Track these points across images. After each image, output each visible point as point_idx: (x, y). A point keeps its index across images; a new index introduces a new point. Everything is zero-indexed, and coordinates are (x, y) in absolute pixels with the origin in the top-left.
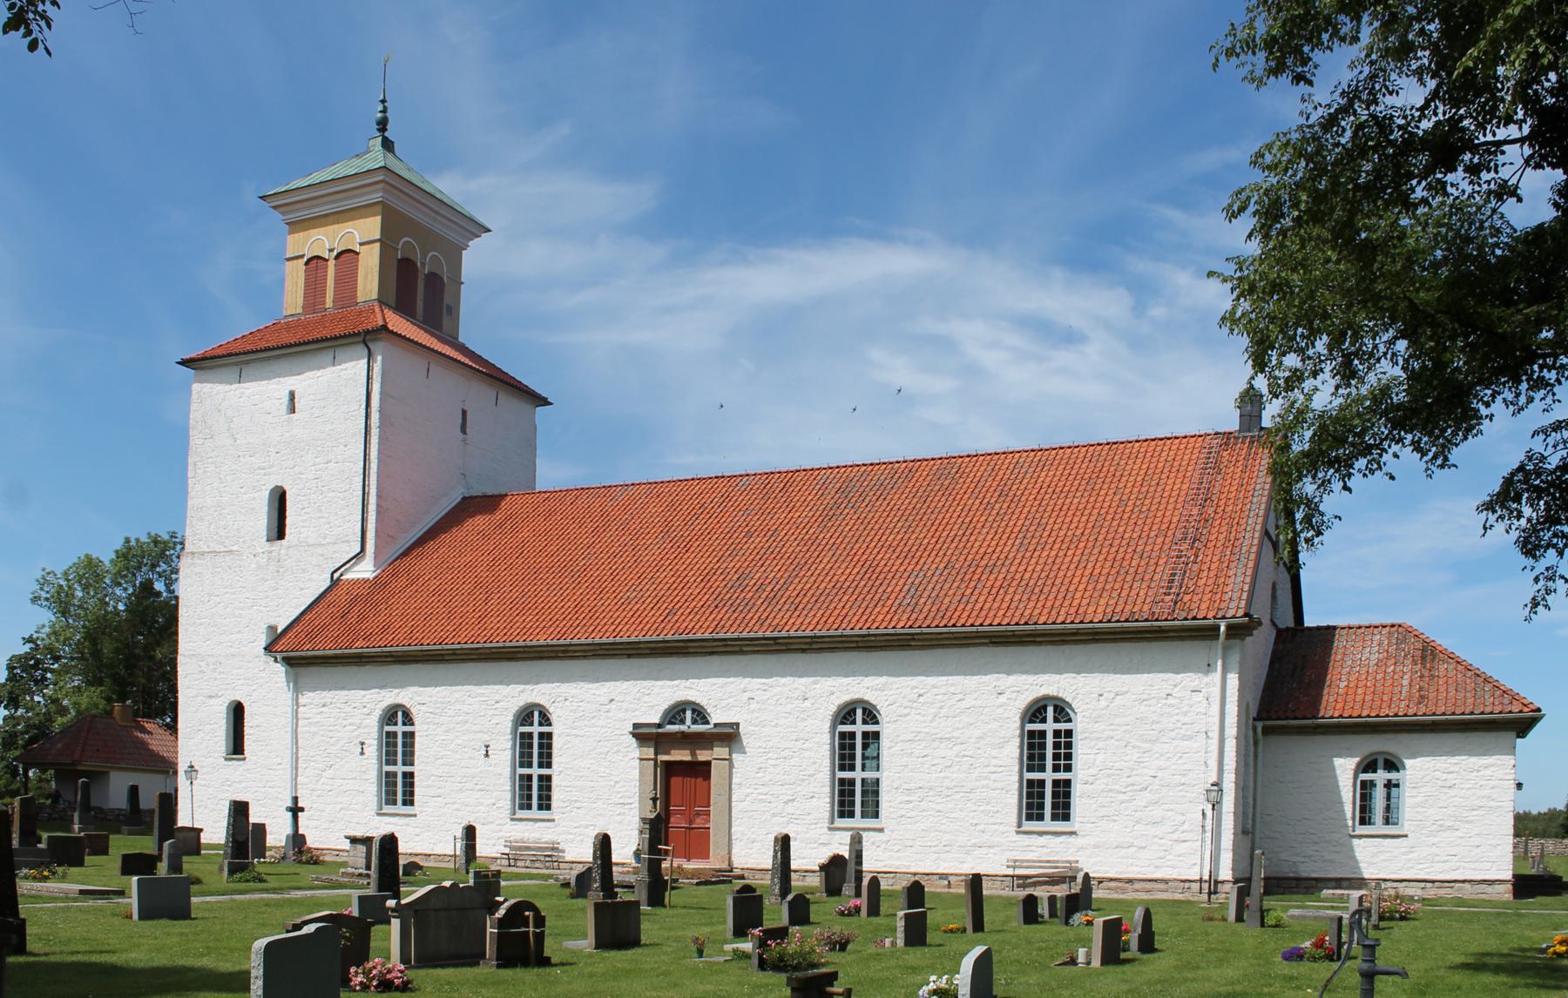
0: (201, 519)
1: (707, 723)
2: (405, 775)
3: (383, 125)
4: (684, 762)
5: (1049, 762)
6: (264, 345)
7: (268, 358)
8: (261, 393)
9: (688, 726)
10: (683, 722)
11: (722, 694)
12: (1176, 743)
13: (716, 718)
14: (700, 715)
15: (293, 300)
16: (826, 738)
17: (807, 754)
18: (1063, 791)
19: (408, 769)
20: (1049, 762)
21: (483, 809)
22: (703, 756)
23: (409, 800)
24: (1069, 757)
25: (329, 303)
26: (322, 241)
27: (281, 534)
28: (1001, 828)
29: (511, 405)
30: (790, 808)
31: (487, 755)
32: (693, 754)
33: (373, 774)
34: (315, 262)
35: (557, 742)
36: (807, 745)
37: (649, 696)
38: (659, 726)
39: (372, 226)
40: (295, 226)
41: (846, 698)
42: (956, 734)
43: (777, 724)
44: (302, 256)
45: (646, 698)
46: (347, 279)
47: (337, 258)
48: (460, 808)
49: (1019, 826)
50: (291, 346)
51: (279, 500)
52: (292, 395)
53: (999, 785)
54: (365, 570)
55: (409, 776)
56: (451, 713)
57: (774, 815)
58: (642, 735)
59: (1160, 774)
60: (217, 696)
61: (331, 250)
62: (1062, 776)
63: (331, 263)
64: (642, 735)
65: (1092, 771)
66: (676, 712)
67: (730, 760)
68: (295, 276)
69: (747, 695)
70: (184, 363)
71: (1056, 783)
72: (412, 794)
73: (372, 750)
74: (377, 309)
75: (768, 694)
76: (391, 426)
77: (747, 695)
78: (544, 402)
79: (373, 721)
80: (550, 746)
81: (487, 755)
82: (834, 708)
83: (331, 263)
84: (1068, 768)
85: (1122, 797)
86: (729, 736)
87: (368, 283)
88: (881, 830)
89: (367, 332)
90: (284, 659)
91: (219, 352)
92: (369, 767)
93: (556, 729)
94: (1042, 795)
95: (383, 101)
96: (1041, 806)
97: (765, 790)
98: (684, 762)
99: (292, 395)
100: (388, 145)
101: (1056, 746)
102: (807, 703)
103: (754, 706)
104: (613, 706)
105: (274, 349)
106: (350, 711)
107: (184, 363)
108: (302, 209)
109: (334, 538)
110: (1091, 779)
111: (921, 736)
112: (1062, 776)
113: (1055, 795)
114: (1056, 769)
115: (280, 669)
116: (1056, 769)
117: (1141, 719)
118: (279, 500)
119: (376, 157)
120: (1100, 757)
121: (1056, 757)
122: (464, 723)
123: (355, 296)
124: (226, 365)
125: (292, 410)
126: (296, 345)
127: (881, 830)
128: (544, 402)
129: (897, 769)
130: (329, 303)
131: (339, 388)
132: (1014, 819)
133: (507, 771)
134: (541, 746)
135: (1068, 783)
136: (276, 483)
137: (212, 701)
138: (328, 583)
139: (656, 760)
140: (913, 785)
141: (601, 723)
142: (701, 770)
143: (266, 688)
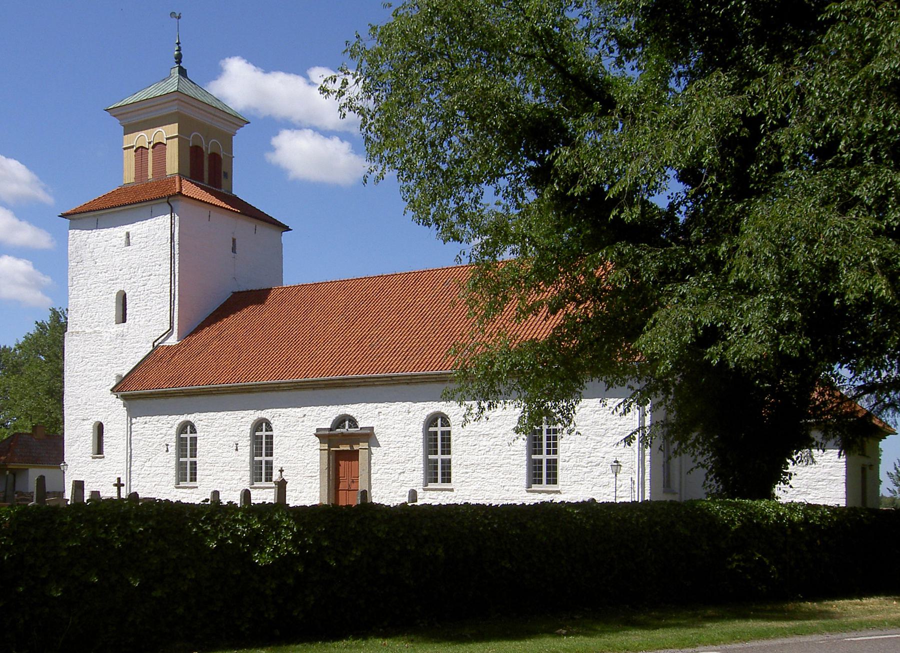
0: (77, 312)
1: (357, 427)
2: (191, 463)
3: (179, 59)
4: (344, 448)
5: (545, 448)
6: (109, 204)
7: (118, 211)
8: (110, 237)
9: (347, 429)
10: (344, 427)
11: (366, 414)
12: (615, 437)
13: (361, 424)
14: (353, 422)
15: (129, 176)
16: (421, 435)
17: (411, 445)
18: (552, 465)
19: (193, 459)
20: (545, 448)
21: (235, 482)
22: (356, 447)
23: (194, 479)
24: (555, 445)
25: (150, 177)
26: (144, 137)
27: (124, 321)
28: (518, 488)
29: (265, 231)
30: (402, 478)
31: (237, 450)
32: (351, 447)
33: (173, 463)
34: (140, 150)
35: (275, 441)
36: (411, 439)
37: (324, 416)
38: (331, 429)
39: (172, 129)
40: (130, 129)
41: (431, 411)
42: (492, 432)
43: (395, 428)
44: (133, 147)
45: (323, 414)
46: (160, 161)
47: (153, 147)
48: (223, 477)
49: (529, 486)
50: (126, 205)
51: (122, 299)
52: (128, 234)
53: (516, 462)
54: (173, 341)
55: (194, 464)
56: (217, 425)
57: (393, 482)
58: (322, 435)
59: (606, 456)
60: (88, 419)
61: (150, 143)
62: (552, 457)
63: (150, 150)
64: (322, 435)
65: (569, 454)
66: (340, 421)
67: (369, 449)
68: (129, 158)
69: (378, 410)
70: (63, 216)
71: (548, 461)
72: (195, 474)
73: (173, 449)
74: (177, 179)
75: (389, 409)
76: (188, 256)
77: (378, 410)
78: (287, 229)
79: (173, 431)
80: (272, 443)
81: (237, 450)
82: (424, 417)
83: (150, 150)
84: (555, 452)
85: (585, 470)
86: (368, 436)
87: (172, 166)
88: (452, 490)
89: (170, 196)
90: (122, 396)
91: (85, 209)
92: (171, 459)
93: (275, 433)
94: (541, 468)
95: (178, 44)
96: (541, 475)
97: (388, 466)
98: (344, 448)
99: (128, 234)
100: (183, 72)
101: (548, 438)
102: (411, 414)
103: (382, 417)
104: (305, 418)
105: (116, 207)
106: (161, 429)
107: (63, 216)
108: (134, 119)
109: (154, 320)
110: (567, 459)
111: (473, 433)
112: (552, 457)
113: (548, 468)
114: (548, 453)
115: (120, 402)
116: (548, 453)
117: (595, 422)
118: (122, 299)
119: (172, 84)
120: (572, 446)
121: (548, 445)
122: (223, 435)
123: (147, 176)
124: (88, 217)
125: (128, 244)
126: (129, 204)
127: (452, 490)
128: (287, 229)
129: (460, 455)
130: (150, 177)
131: (155, 233)
132: (524, 482)
133: (248, 459)
134: (267, 443)
135: (555, 461)
136: (124, 288)
137: (85, 422)
138: (151, 348)
139: (329, 450)
140: (468, 463)
141: (299, 429)
142: (353, 455)
143: (114, 413)
